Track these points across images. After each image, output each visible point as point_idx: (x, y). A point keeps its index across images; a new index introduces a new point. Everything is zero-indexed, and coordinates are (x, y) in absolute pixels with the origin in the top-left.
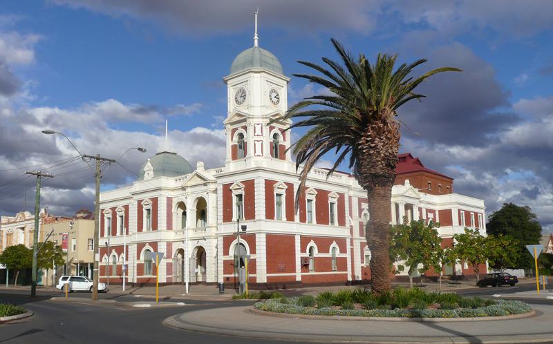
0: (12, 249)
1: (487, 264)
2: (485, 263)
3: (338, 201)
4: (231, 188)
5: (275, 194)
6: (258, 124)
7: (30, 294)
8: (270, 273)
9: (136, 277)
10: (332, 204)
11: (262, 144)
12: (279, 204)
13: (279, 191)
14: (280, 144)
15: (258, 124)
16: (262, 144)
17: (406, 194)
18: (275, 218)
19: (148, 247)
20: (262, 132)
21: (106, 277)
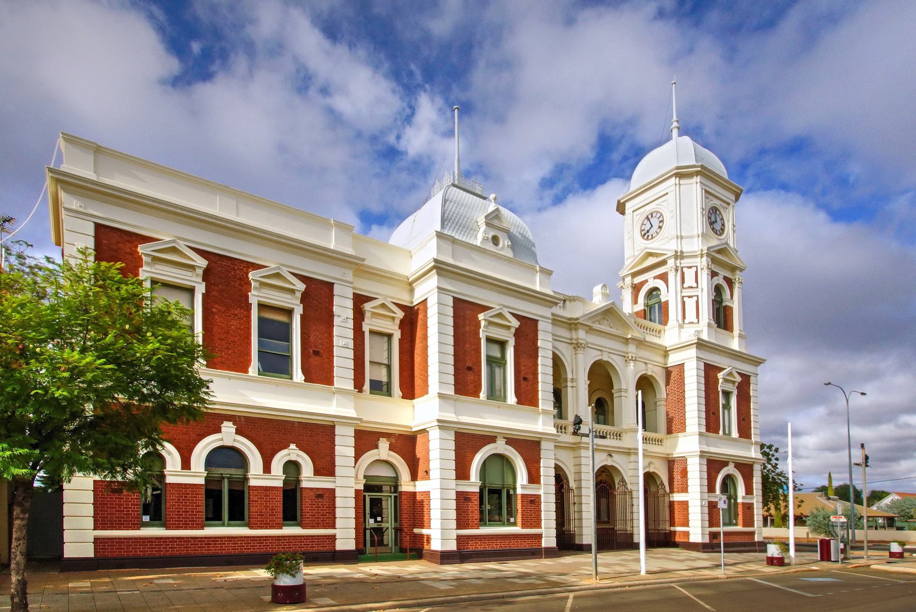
0: (560, 474)
1: (818, 498)
2: (817, 499)
3: (303, 300)
4: (142, 249)
5: (482, 335)
6: (690, 267)
7: (577, 542)
8: (527, 527)
9: (454, 533)
10: (727, 394)
11: (697, 302)
12: (727, 406)
13: (729, 387)
14: (724, 304)
15: (690, 267)
16: (697, 302)
17: (63, 214)
18: (483, 395)
19: (730, 469)
20: (697, 281)
21: (517, 530)
